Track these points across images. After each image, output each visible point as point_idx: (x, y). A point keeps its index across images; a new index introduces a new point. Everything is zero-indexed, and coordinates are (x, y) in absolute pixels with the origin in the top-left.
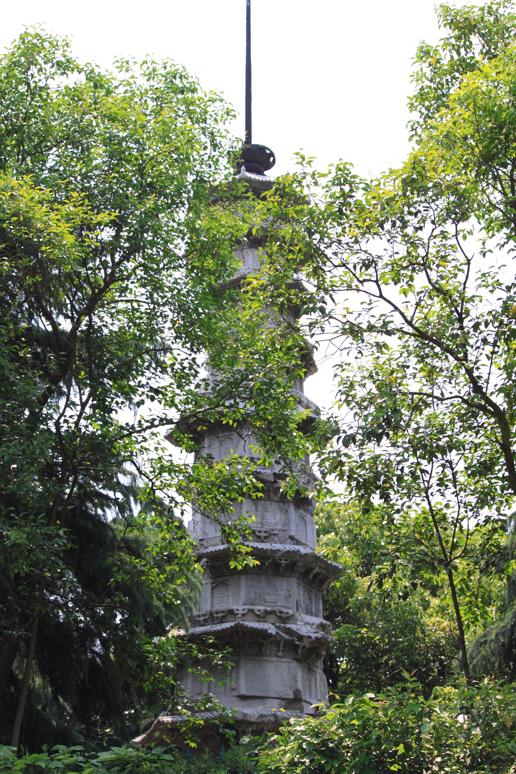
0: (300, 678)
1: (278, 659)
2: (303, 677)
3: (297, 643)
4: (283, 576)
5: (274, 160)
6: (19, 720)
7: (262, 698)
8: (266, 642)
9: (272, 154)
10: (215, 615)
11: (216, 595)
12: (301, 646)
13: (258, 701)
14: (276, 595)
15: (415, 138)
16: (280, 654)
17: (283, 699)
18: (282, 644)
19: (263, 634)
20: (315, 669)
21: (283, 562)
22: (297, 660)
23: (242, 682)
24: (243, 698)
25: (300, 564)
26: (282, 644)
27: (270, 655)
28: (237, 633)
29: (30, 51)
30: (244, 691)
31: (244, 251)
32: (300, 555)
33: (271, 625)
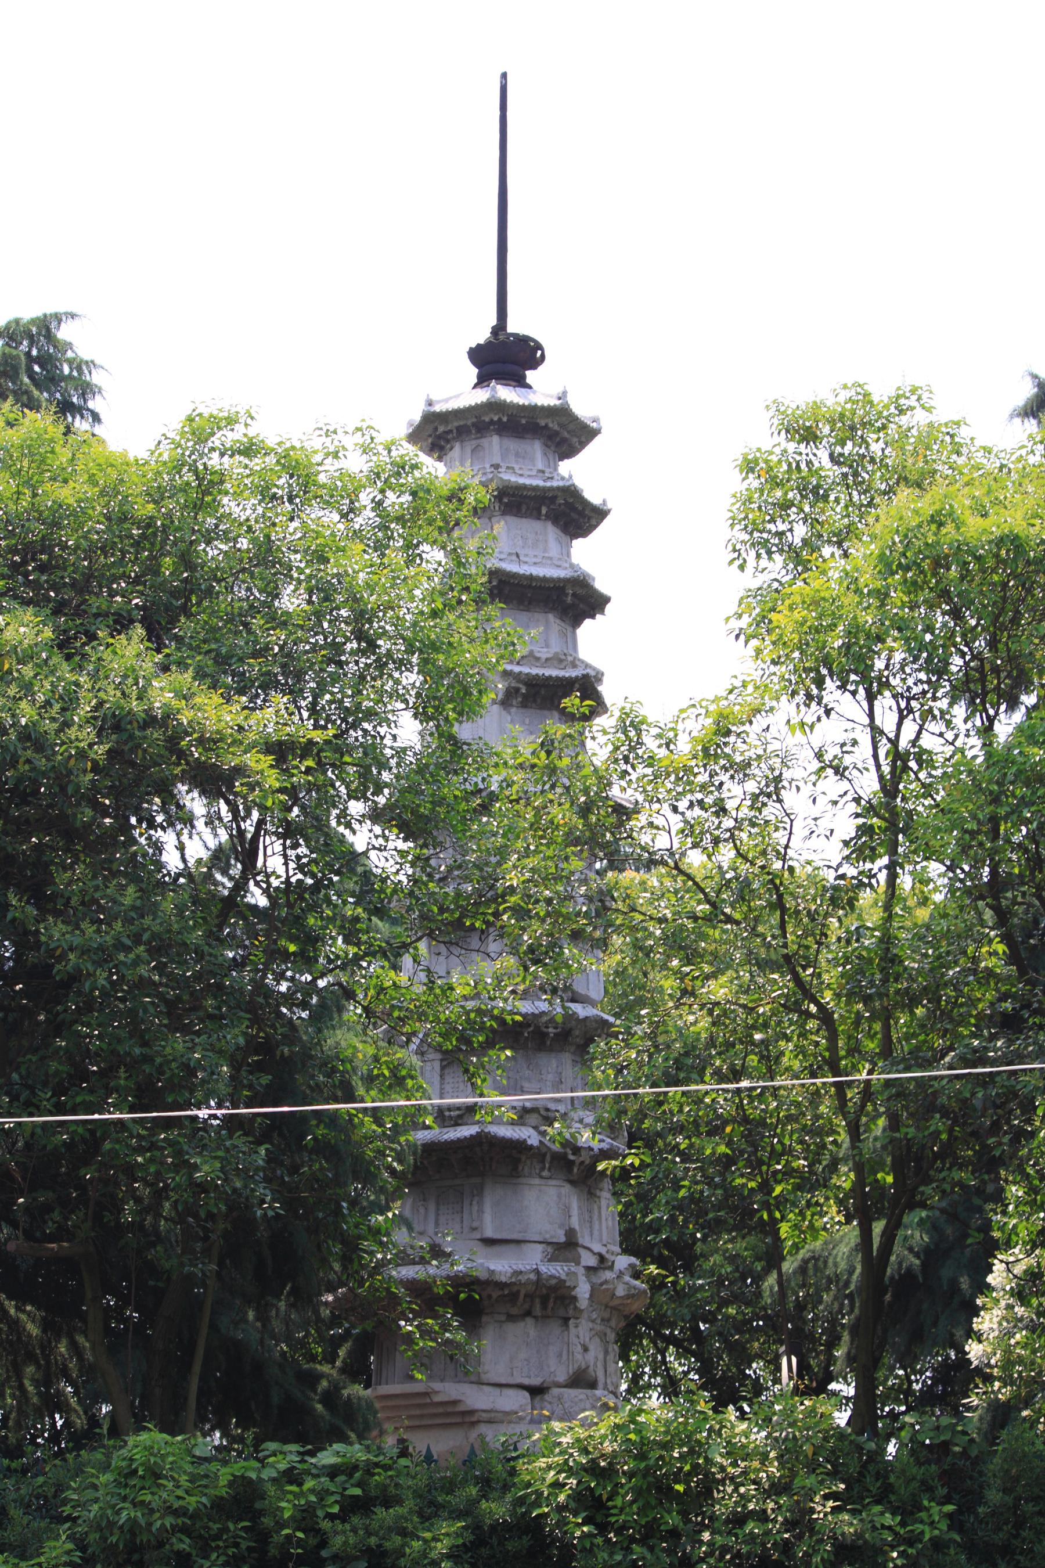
0: (575, 1212)
1: (543, 1182)
2: (580, 1208)
3: (572, 1157)
4: (551, 1050)
5: (543, 356)
6: (197, 1368)
7: (518, 1242)
8: (523, 1158)
9: (539, 346)
10: (447, 1113)
11: (448, 1079)
12: (577, 1162)
13: (512, 1246)
14: (540, 1080)
15: (737, 563)
16: (545, 1173)
17: (549, 1243)
18: (548, 1158)
19: (520, 1146)
20: (598, 1193)
21: (551, 1030)
22: (572, 1182)
23: (487, 1217)
24: (489, 1242)
25: (577, 1033)
26: (548, 1158)
27: (530, 1176)
28: (481, 1144)
29: (200, 430)
30: (489, 1233)
31: (494, 520)
32: (578, 1020)
33: (531, 1130)
